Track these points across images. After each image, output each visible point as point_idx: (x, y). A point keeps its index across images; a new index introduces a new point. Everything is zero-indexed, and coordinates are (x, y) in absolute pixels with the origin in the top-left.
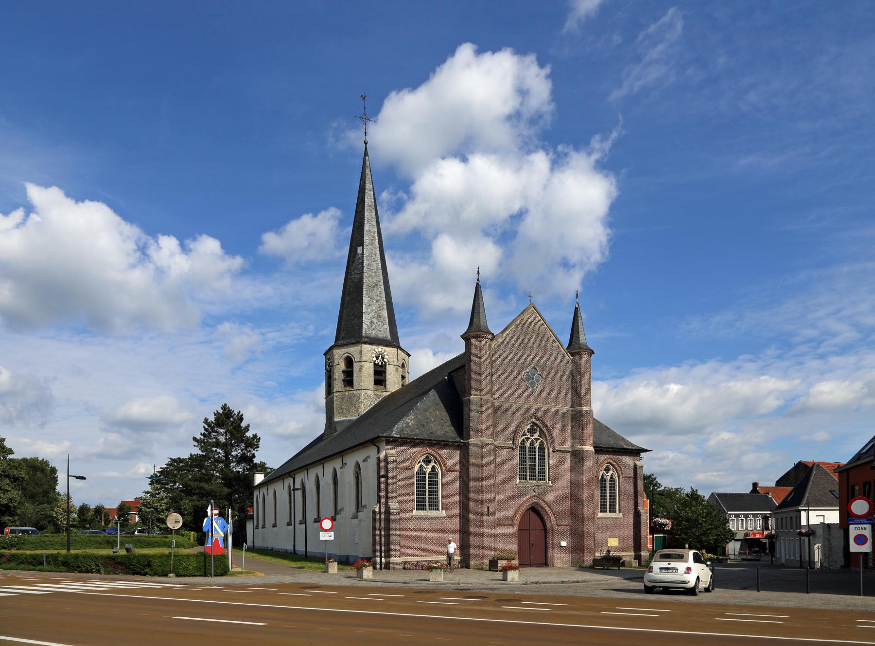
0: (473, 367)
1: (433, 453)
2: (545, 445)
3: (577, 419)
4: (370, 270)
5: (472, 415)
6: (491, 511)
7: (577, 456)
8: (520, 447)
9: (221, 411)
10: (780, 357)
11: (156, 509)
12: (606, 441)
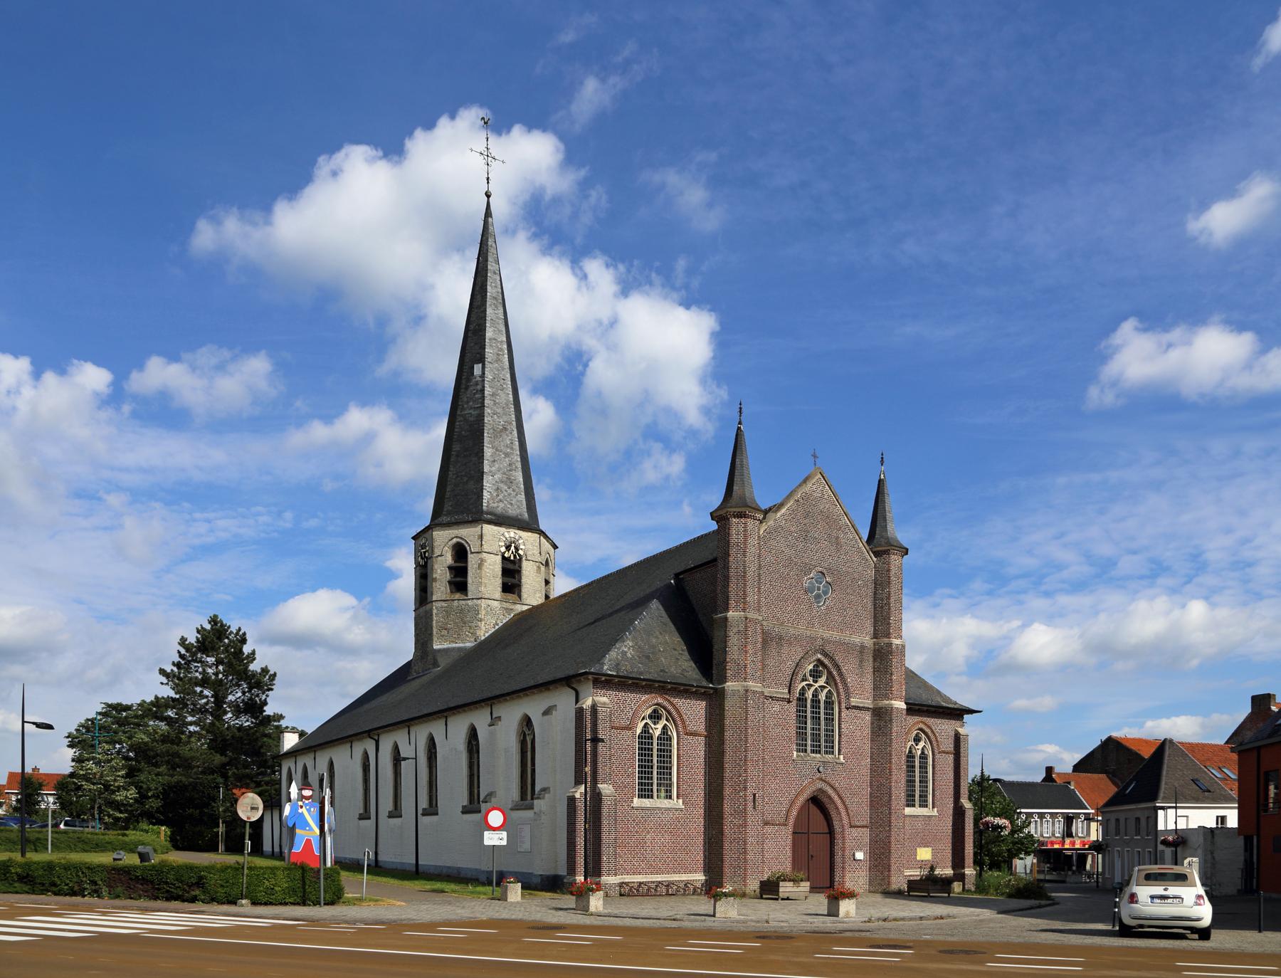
0: (732, 565)
1: (666, 704)
3: (883, 657)
4: (495, 403)
5: (729, 644)
6: (759, 801)
7: (881, 716)
8: (799, 699)
9: (208, 627)
10: (990, 593)
11: (107, 787)
12: (925, 698)
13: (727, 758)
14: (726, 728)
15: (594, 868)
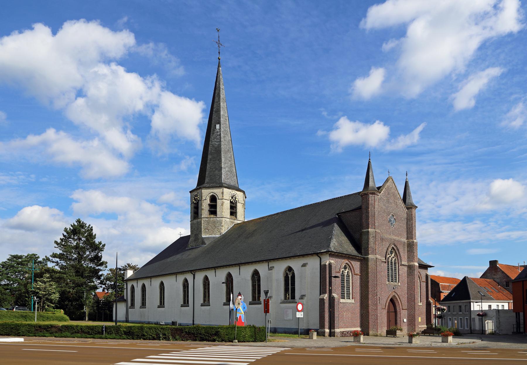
0: (370, 212)
1: (349, 263)
2: (397, 261)
3: (411, 247)
5: (370, 241)
7: (410, 268)
9: (76, 224)
13: (370, 284)
14: (369, 272)
15: (332, 326)
